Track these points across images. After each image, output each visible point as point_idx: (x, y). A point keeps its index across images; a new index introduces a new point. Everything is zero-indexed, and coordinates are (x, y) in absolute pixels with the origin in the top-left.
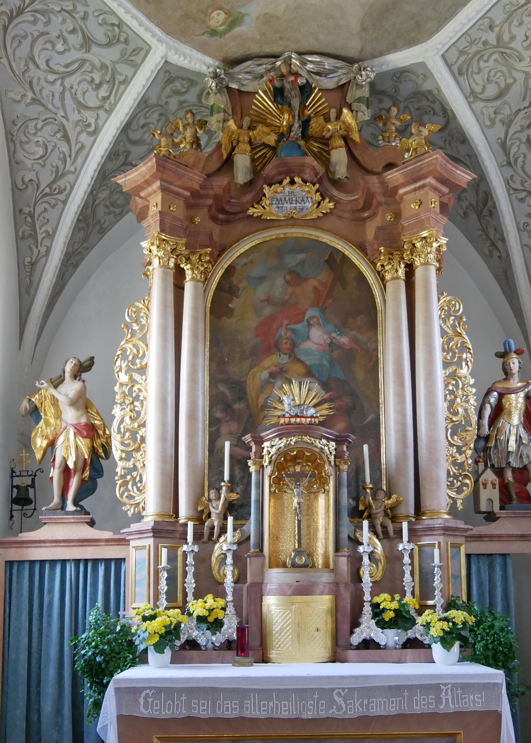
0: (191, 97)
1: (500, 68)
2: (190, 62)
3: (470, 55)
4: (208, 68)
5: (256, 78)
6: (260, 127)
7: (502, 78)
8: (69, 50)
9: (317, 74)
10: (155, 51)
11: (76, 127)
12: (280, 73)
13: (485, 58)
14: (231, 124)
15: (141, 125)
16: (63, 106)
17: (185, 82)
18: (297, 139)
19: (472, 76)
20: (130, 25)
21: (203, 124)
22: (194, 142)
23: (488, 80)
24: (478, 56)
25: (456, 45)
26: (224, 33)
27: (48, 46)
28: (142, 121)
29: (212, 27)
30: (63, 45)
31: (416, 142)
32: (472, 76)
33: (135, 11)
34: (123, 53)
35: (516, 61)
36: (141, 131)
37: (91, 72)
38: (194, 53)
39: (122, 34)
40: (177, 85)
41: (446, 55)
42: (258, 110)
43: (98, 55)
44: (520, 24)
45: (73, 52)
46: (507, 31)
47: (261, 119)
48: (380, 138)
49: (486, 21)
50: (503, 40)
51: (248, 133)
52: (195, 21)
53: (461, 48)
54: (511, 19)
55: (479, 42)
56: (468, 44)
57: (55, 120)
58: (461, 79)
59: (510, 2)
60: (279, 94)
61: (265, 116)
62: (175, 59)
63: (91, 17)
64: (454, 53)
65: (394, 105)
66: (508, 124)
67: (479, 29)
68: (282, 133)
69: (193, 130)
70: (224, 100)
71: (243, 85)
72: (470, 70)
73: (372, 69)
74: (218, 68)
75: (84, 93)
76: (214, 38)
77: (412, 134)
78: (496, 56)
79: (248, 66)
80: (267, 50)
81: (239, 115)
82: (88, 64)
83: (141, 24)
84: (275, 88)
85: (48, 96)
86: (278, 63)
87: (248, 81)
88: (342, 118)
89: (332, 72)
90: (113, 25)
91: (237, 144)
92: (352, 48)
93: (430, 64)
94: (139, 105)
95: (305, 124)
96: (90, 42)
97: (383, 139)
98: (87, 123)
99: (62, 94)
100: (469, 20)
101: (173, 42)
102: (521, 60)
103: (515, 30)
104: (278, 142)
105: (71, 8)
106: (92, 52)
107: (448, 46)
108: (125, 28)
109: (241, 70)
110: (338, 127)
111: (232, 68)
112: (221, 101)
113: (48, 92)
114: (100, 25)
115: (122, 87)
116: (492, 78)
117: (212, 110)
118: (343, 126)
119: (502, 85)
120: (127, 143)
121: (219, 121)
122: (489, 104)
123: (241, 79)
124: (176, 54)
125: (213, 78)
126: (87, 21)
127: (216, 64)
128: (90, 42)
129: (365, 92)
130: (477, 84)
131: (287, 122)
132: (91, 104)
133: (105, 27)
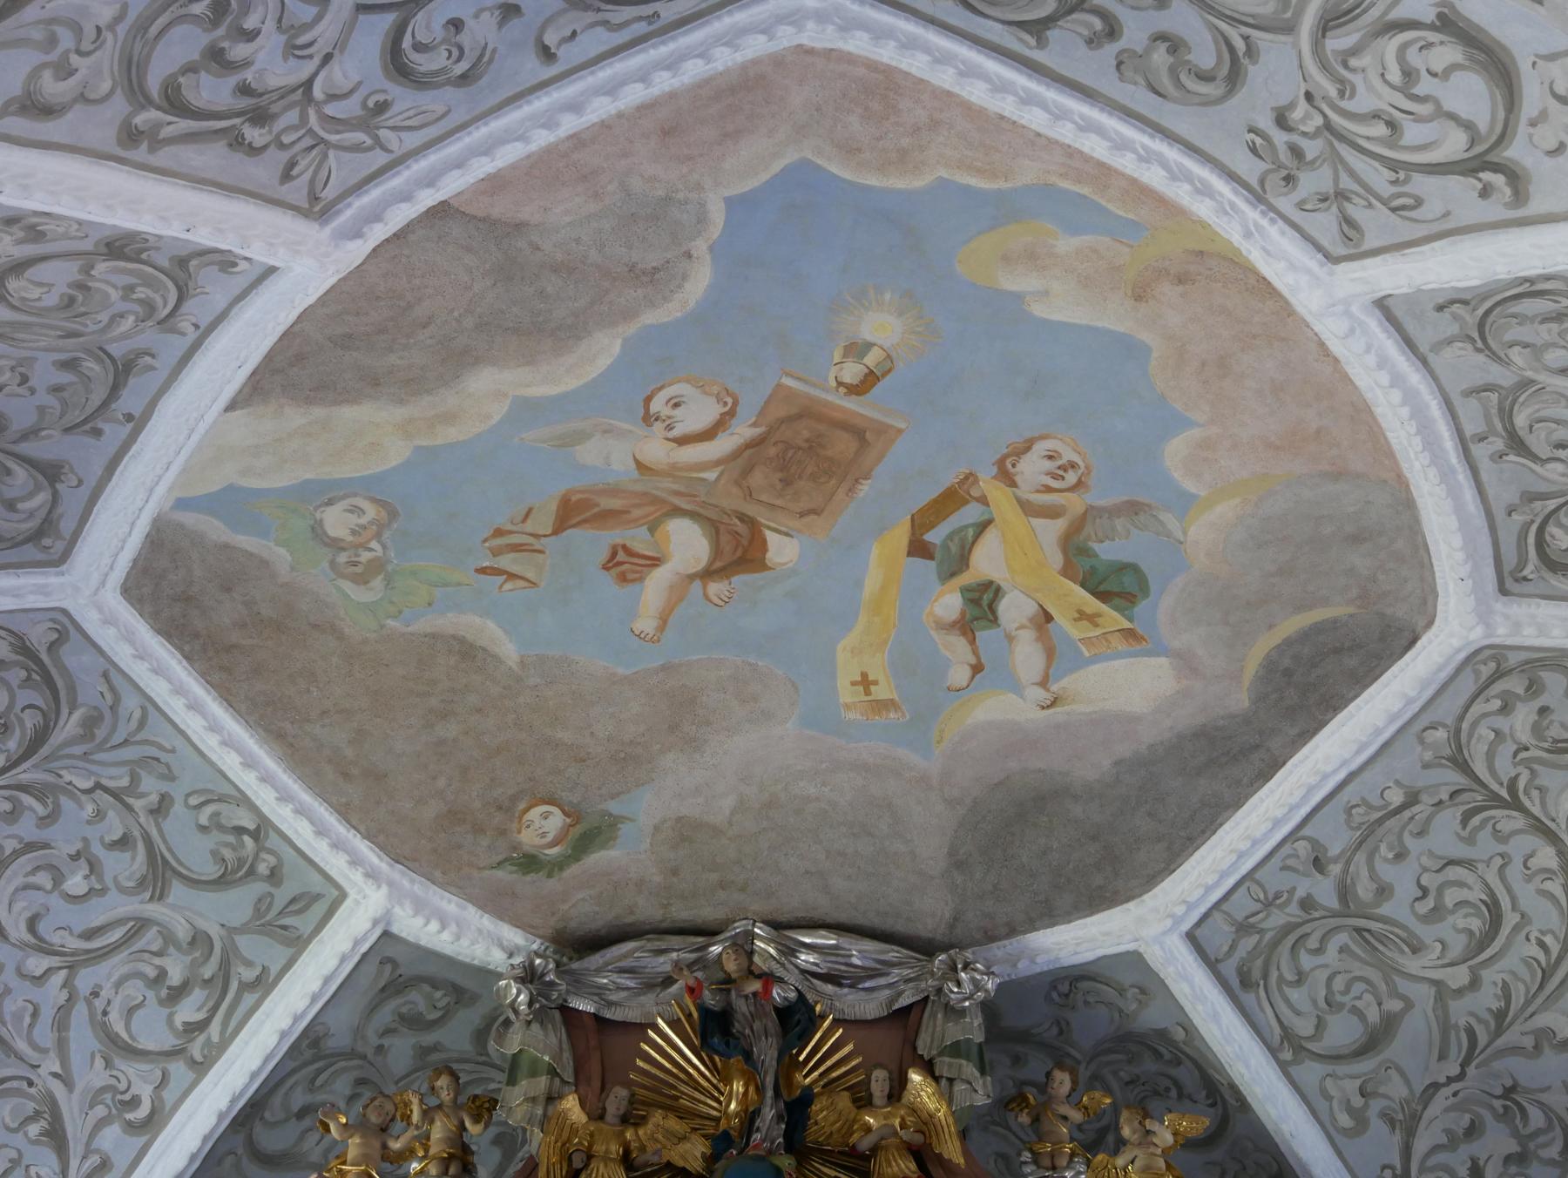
0: (456, 1036)
1: (1359, 970)
2: (458, 938)
3: (1268, 936)
4: (511, 956)
5: (649, 986)
6: (657, 1117)
7: (1368, 997)
8: (103, 891)
9: (828, 978)
10: (357, 902)
11: (91, 1107)
12: (721, 975)
13: (1313, 943)
14: (571, 1105)
15: (295, 1108)
16: (62, 1046)
17: (438, 994)
18: (770, 1152)
19: (1280, 990)
20: (289, 833)
21: (484, 1108)
22: (451, 1157)
23: (1328, 1003)
24: (1292, 938)
25: (1224, 907)
26: (560, 864)
27: (44, 879)
28: (299, 1099)
29: (526, 848)
30: (86, 877)
31: (1138, 1163)
32: (1280, 990)
33: (306, 797)
34: (261, 906)
35: (1402, 952)
36: (294, 1128)
37: (159, 954)
38: (472, 913)
39: (264, 855)
40: (417, 999)
41: (1198, 933)
42: (654, 1071)
43: (183, 910)
44: (1400, 856)
45: (113, 893)
46: (1364, 873)
47: (662, 1095)
48: (1026, 1156)
49: (1302, 847)
50: (1356, 894)
51: (622, 1133)
52: (478, 830)
53: (1239, 917)
54: (1370, 842)
55: (1288, 901)
56: (1259, 906)
57: (31, 1084)
58: (1248, 999)
59: (1363, 799)
60: (714, 1029)
61: (675, 1088)
62: (417, 928)
63: (178, 808)
64: (1221, 926)
65: (1060, 1065)
66: (1407, 1124)
67: (1284, 868)
68: (726, 1134)
69: (452, 1125)
70: (553, 1040)
71: (610, 1004)
72: (1274, 975)
73: (988, 968)
74: (537, 954)
75: (131, 1011)
76: (528, 878)
77: (1121, 1143)
78: (1343, 938)
79: (625, 956)
80: (682, 913)
81: (597, 1084)
82: (152, 932)
83: (321, 832)
84: (705, 1012)
85: (18, 1017)
86: (716, 949)
87: (624, 994)
88: (908, 1097)
89: (873, 974)
90: (240, 830)
91: (586, 1166)
92: (930, 911)
93: (1154, 956)
94: (295, 1047)
95: (797, 1110)
96: (169, 874)
97: (1036, 1162)
98: (127, 1097)
99: (64, 1011)
100: (1255, 843)
101: (412, 881)
102: (1415, 951)
103: (1387, 872)
104: (711, 1159)
105: (125, 782)
106: (171, 900)
107: (1203, 909)
108: (273, 841)
109: (607, 964)
110: (897, 1122)
111: (580, 958)
112: (542, 1044)
113: (20, 1003)
114: (203, 829)
115: (249, 999)
116: (1339, 998)
117: (514, 1069)
118: (910, 1119)
119: (1373, 1015)
120: (245, 1160)
121: (533, 1100)
122: (1342, 1069)
123: (603, 987)
124: (416, 914)
125: (522, 980)
126: (165, 817)
127: (535, 947)
128: (169, 874)
129: (973, 1029)
130: (1298, 1013)
131: (738, 1103)
132: (146, 1043)
133: (216, 837)
